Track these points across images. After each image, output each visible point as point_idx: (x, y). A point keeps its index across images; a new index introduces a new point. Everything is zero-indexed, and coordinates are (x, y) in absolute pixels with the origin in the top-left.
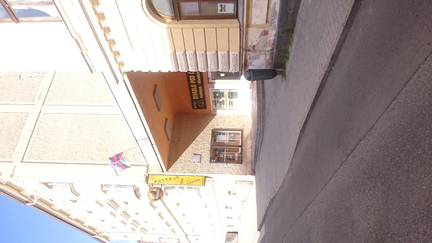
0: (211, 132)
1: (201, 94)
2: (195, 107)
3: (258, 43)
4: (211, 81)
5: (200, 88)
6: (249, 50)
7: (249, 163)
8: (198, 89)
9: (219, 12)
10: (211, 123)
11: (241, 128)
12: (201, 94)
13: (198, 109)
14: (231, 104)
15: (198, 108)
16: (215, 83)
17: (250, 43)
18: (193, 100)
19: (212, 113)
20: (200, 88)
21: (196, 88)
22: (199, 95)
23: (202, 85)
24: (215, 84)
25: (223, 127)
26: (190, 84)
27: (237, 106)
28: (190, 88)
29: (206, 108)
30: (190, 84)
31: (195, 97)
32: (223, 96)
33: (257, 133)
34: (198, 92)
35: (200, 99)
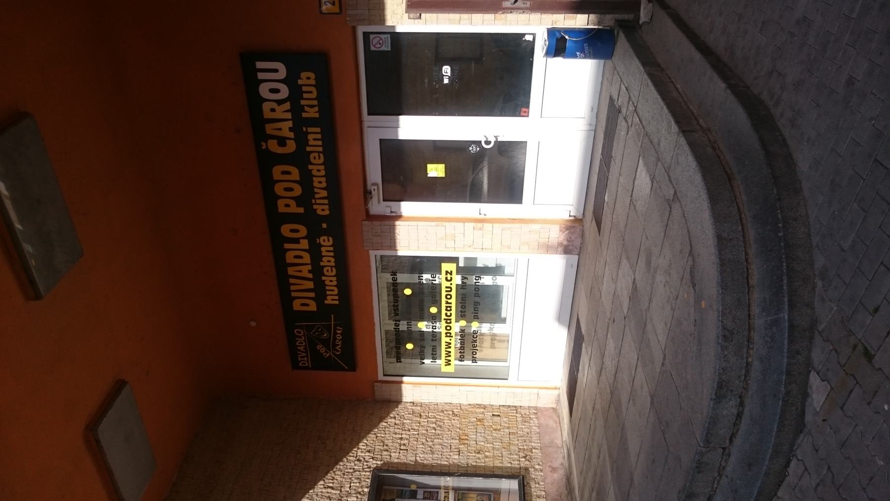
0: (366, 478)
1: (330, 280)
2: (305, 360)
4: (378, 207)
5: (326, 242)
8: (315, 252)
10: (371, 436)
11: (515, 464)
12: (330, 280)
13: (314, 368)
14: (468, 345)
15: (320, 363)
16: (399, 217)
18: (292, 318)
19: (381, 392)
20: (326, 242)
21: (305, 244)
22: (320, 290)
23: (336, 225)
24: (403, 386)
25: (425, 458)
26: (276, 219)
28: (278, 244)
31: (303, 303)
32: (437, 303)
33: (713, 421)
34: (317, 271)
35: (324, 311)
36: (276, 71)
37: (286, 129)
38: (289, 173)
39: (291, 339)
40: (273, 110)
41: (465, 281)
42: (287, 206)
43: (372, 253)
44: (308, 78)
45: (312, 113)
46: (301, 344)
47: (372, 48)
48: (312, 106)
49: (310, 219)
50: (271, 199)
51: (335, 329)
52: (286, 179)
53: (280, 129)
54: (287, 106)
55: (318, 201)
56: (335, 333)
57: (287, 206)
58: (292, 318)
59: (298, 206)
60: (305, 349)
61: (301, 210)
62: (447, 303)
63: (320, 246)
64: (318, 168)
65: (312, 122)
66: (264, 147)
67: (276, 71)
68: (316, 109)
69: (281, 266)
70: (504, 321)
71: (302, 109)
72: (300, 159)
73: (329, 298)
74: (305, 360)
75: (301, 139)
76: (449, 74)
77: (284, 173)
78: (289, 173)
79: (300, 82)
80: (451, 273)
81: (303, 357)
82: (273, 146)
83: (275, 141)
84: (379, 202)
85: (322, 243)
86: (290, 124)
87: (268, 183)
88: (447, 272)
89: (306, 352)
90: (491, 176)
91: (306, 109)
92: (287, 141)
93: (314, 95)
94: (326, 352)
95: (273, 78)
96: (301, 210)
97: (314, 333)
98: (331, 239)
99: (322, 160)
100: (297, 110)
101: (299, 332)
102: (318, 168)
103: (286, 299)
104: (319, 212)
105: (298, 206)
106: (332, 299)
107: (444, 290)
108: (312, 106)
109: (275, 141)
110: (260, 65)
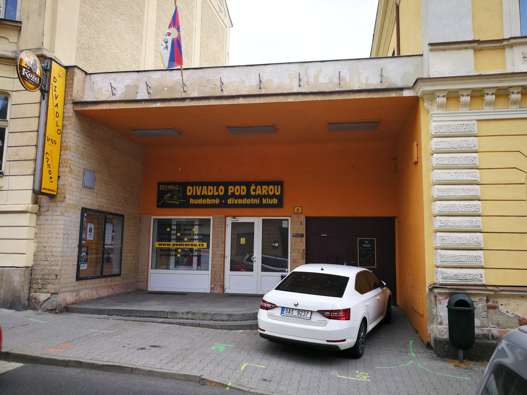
3: (502, 314)
6: (487, 301)
7: (77, 295)
8: (213, 197)
9: (211, 218)
12: (201, 201)
17: (501, 301)
21: (216, 194)
22: (196, 197)
27: (495, 300)
28: (217, 184)
29: (158, 206)
30: (226, 185)
31: (190, 191)
34: (205, 197)
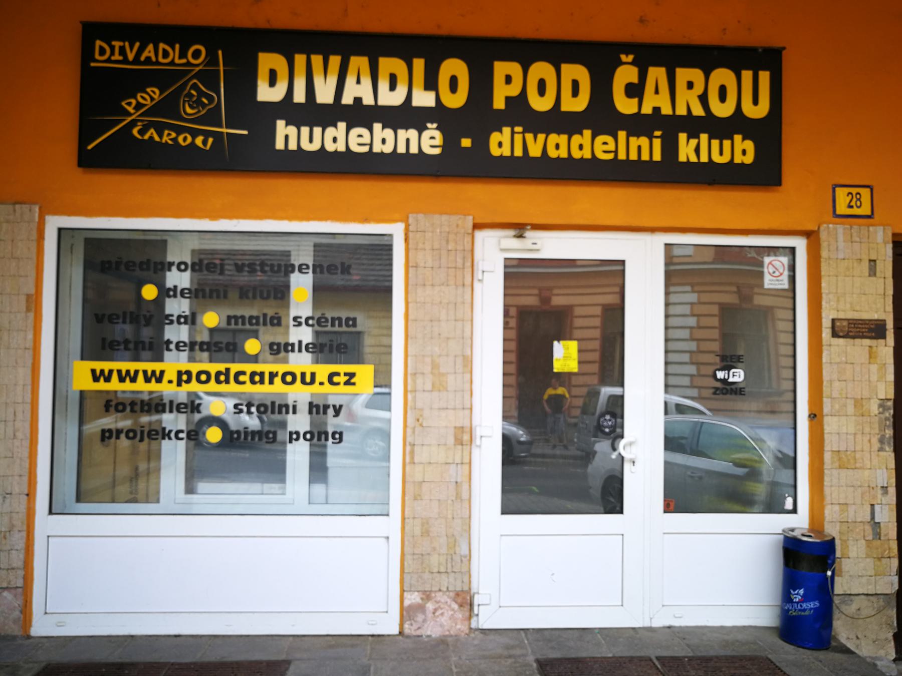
1: (336, 138)
5: (430, 141)
8: (404, 117)
12: (336, 138)
20: (430, 141)
26: (481, 53)
28: (426, 49)
34: (360, 115)
36: (756, 102)
37: (655, 100)
38: (575, 92)
39: (183, 35)
40: (690, 85)
41: (331, 411)
42: (508, 80)
43: (396, 230)
44: (744, 152)
45: (686, 150)
46: (166, 55)
47: (767, 260)
48: (697, 150)
49: (477, 117)
50: (526, 51)
51: (207, 134)
52: (567, 87)
53: (657, 92)
54: (698, 111)
55: (518, 138)
56: (194, 133)
57: (508, 80)
58: (240, 48)
59: (508, 99)
60: (148, 60)
61: (499, 104)
62: (273, 376)
63: (421, 129)
64: (585, 145)
65: (671, 148)
66: (623, 58)
67: (756, 102)
68: (693, 159)
69: (374, 45)
70: (190, 489)
71: (693, 134)
72: (601, 117)
73: (292, 130)
74: (109, 55)
75: (639, 125)
76: (731, 380)
77: (575, 85)
78: (575, 92)
79: (738, 138)
80: (347, 383)
81: (122, 51)
82: (626, 74)
83: (635, 80)
84: (503, 250)
85: (426, 134)
86: (666, 110)
87: (558, 52)
88: (352, 375)
89: (136, 61)
90: (558, 454)
91: (693, 142)
92: (636, 100)
93: (716, 158)
94: (139, 106)
95: (740, 94)
96: (499, 104)
97: (195, 87)
98: (437, 151)
99: (601, 156)
100: (692, 126)
101: (196, 54)
102: (585, 145)
103: (294, 42)
104: (495, 138)
105: (508, 99)
106: (286, 135)
107: (157, 366)
108: (697, 150)
109: (635, 80)
110: (765, 77)
